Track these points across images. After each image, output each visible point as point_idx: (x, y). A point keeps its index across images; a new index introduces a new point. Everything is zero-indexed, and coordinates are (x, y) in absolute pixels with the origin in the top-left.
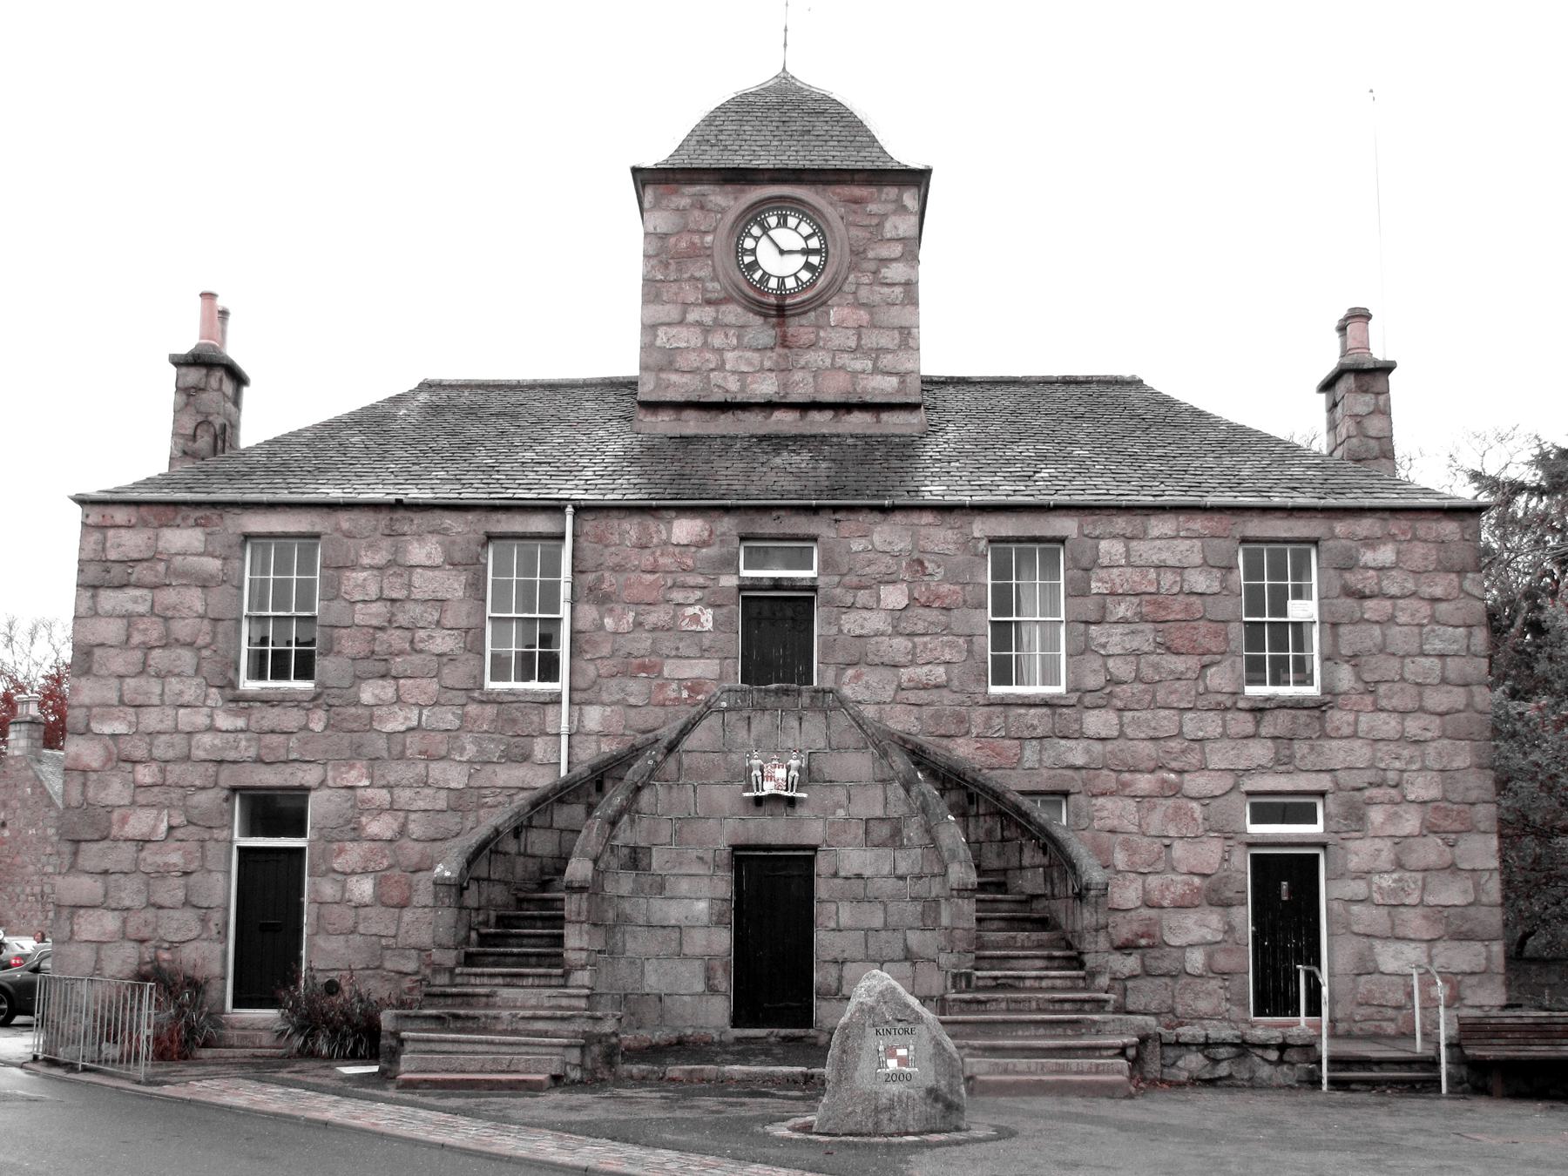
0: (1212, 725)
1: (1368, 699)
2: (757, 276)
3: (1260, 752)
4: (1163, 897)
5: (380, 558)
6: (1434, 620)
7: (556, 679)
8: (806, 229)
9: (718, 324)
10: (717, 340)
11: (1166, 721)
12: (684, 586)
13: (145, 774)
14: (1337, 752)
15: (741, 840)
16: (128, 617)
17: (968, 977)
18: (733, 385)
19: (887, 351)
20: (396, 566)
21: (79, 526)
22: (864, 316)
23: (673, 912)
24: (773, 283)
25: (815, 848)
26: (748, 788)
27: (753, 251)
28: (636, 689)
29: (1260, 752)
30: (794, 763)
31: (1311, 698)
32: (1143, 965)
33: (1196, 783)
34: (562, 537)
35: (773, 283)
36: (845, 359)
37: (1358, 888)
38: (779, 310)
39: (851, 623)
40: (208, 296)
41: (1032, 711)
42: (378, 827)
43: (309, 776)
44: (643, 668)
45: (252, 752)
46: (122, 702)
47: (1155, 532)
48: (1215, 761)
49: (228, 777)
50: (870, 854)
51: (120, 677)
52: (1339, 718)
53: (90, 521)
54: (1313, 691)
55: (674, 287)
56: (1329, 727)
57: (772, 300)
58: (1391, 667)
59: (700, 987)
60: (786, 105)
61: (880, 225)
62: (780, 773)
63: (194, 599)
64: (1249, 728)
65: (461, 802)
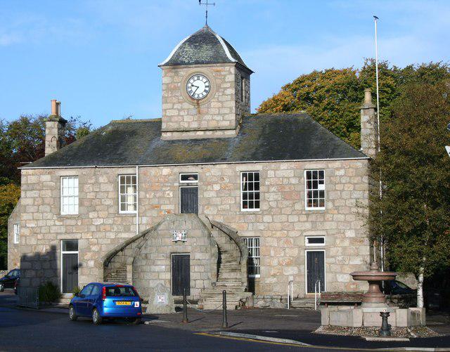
0: (296, 219)
1: (336, 211)
3: (308, 225)
5: (93, 181)
6: (354, 189)
7: (64, 254)
8: (205, 80)
9: (182, 109)
10: (182, 113)
11: (284, 218)
12: (166, 186)
13: (40, 237)
14: (328, 225)
18: (186, 126)
19: (227, 114)
20: (97, 183)
22: (220, 105)
23: (157, 268)
28: (154, 213)
29: (308, 225)
30: (183, 232)
32: (32, 266)
33: (292, 234)
36: (215, 117)
38: (197, 102)
39: (207, 195)
42: (94, 248)
43: (78, 236)
44: (156, 207)
46: (33, 219)
47: (282, 168)
49: (60, 237)
50: (201, 254)
52: (328, 216)
56: (326, 218)
58: (342, 203)
61: (224, 79)
62: (180, 235)
63: (49, 193)
64: (305, 219)
65: (113, 240)
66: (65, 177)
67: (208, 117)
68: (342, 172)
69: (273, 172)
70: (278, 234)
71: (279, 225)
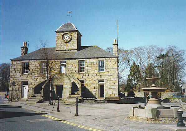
10: (61, 45)
43: (28, 80)
49: (98, 79)
68: (109, 61)
69: (88, 61)
70: (90, 79)
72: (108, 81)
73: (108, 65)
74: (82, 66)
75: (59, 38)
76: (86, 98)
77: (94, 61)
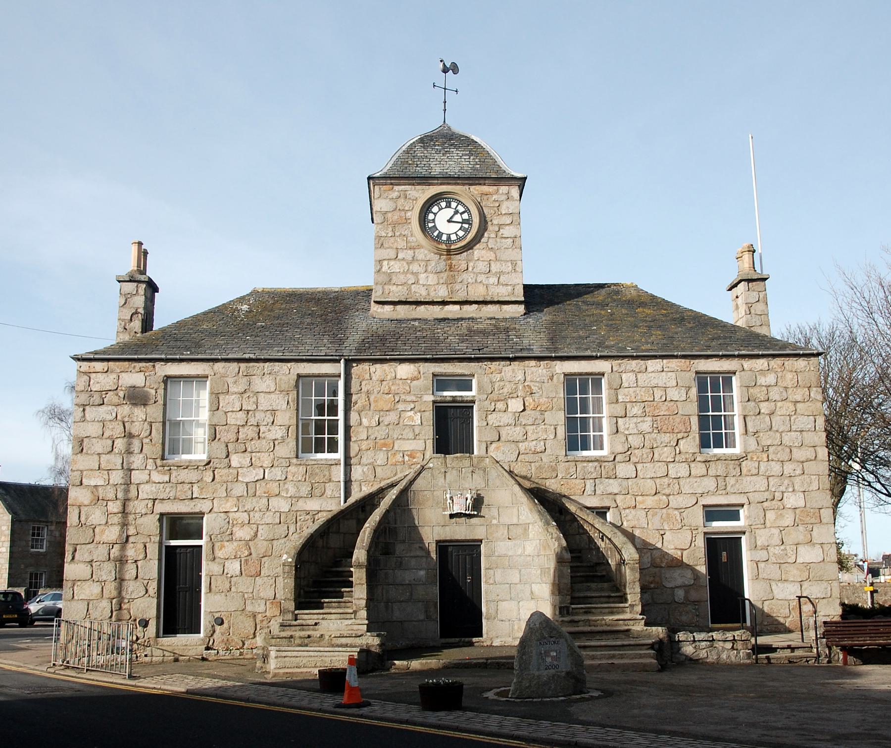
0: (680, 470)
1: (765, 456)
2: (436, 234)
3: (709, 484)
4: (662, 562)
7: (337, 452)
10: (415, 267)
15: (442, 538)
16: (103, 422)
17: (568, 608)
21: (76, 373)
22: (491, 255)
24: (444, 238)
25: (481, 541)
26: (444, 509)
27: (434, 221)
29: (709, 484)
31: (736, 455)
32: (653, 599)
33: (675, 501)
34: (339, 376)
35: (444, 238)
37: (763, 555)
40: (140, 244)
41: (591, 464)
43: (204, 506)
45: (172, 495)
48: (686, 489)
49: (161, 508)
51: (99, 454)
53: (82, 370)
54: (737, 450)
55: (392, 239)
57: (444, 247)
59: (422, 617)
60: (445, 139)
66: (188, 378)
67: (468, 277)
68: (770, 379)
69: (632, 377)
70: (650, 501)
71: (649, 486)
72: (770, 515)
73: (765, 408)
74: (584, 410)
75: (395, 225)
76: (327, 600)
77: (668, 379)
